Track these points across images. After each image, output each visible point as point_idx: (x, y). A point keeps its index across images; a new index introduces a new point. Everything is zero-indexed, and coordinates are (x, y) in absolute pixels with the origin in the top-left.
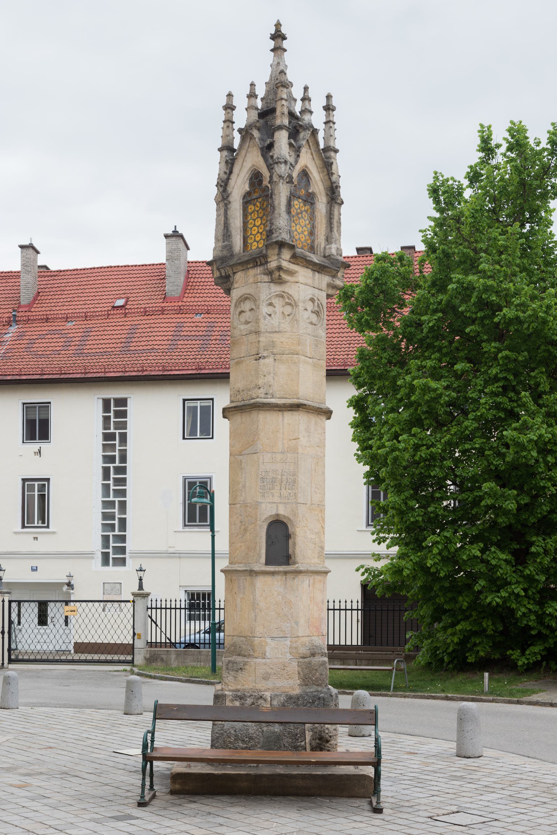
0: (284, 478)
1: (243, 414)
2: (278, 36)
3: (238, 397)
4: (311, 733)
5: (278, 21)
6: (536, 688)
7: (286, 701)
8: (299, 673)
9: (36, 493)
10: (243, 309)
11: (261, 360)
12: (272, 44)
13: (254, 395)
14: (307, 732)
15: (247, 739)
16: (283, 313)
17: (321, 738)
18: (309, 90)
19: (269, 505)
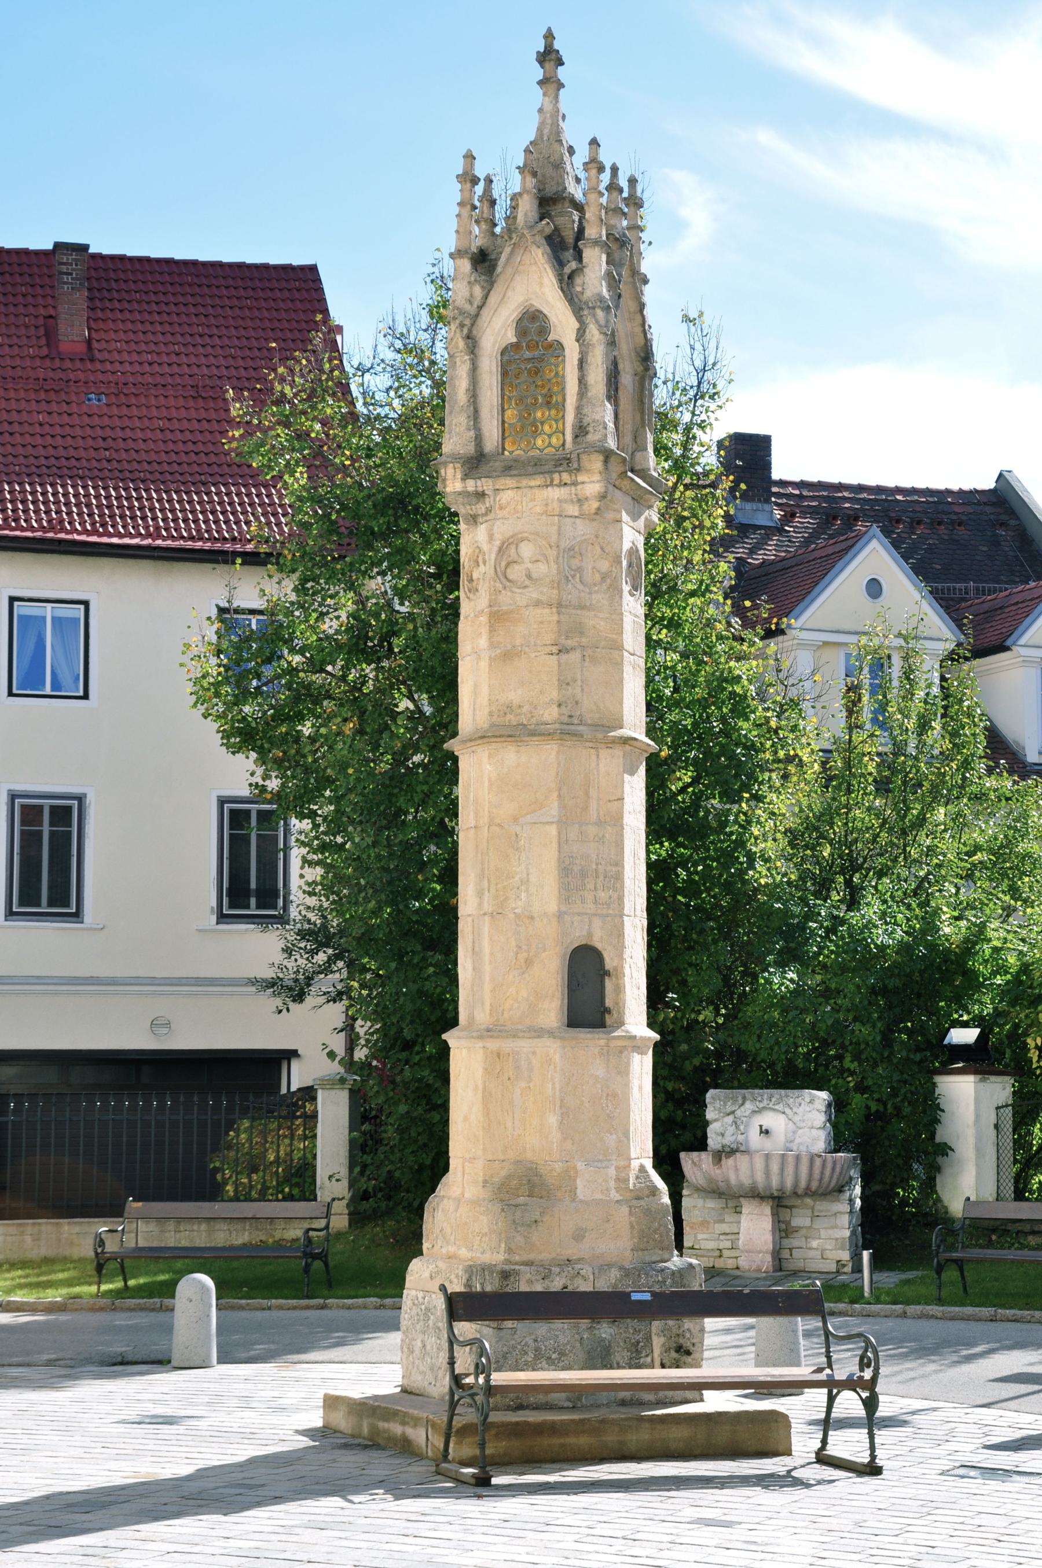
1: (523, 749)
3: (509, 717)
4: (662, 1340)
5: (549, 30)
9: (46, 829)
10: (516, 558)
12: (539, 73)
14: (655, 1338)
17: (679, 1349)
19: (576, 918)
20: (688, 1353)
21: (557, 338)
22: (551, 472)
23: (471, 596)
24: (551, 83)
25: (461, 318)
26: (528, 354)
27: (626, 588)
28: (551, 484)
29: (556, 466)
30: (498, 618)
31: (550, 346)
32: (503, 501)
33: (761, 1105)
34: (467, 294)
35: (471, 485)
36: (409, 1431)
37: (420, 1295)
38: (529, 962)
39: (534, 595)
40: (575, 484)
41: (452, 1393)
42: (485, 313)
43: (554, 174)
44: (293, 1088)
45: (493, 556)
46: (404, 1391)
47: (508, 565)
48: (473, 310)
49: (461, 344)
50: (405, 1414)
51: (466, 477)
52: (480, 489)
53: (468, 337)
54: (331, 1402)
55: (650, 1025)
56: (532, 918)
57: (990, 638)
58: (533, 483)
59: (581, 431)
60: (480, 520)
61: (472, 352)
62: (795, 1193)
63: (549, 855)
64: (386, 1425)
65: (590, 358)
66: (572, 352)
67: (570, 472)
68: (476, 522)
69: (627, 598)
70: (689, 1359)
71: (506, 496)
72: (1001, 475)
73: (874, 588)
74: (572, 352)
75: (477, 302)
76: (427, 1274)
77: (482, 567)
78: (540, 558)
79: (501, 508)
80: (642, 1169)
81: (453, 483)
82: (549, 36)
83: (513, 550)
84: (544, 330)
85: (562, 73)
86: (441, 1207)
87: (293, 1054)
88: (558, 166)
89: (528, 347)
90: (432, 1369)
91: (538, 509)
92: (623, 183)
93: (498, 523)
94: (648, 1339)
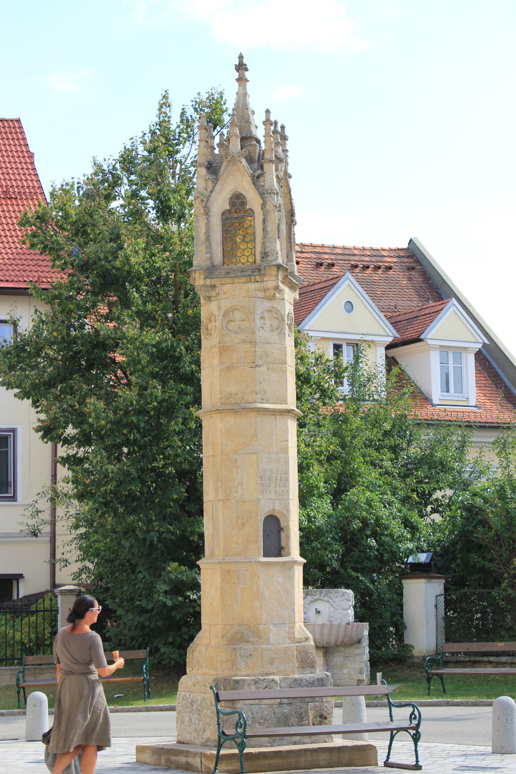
0: (279, 476)
2: (241, 67)
3: (230, 400)
4: (313, 712)
5: (241, 53)
6: (410, 690)
7: (292, 683)
8: (297, 657)
10: (232, 318)
11: (257, 368)
13: (250, 400)
14: (310, 711)
15: (262, 721)
16: (271, 326)
17: (321, 716)
18: (286, 129)
20: (326, 718)
21: (251, 207)
22: (250, 276)
23: (208, 337)
24: (242, 80)
25: (202, 197)
26: (235, 215)
27: (287, 332)
28: (250, 282)
29: (253, 272)
30: (223, 349)
31: (247, 211)
32: (225, 290)
33: (315, 598)
34: (204, 185)
35: (208, 282)
36: (190, 760)
37: (187, 694)
38: (243, 524)
39: (243, 338)
40: (262, 281)
41: (219, 737)
42: (213, 194)
43: (246, 125)
44: (21, 596)
45: (221, 318)
46: (179, 742)
47: (228, 322)
48: (207, 193)
49: (202, 210)
50: (188, 752)
51: (206, 278)
52: (213, 284)
53: (205, 207)
54: (140, 749)
55: (302, 555)
56: (245, 502)
57: (410, 334)
58: (241, 281)
59: (265, 255)
60: (213, 299)
61: (208, 214)
62: (336, 645)
63: (254, 469)
64: (176, 758)
65: (269, 218)
66: (259, 215)
67: (260, 275)
68: (210, 300)
69: (287, 337)
70: (326, 721)
71: (227, 287)
72: (411, 240)
73: (349, 306)
74: (259, 215)
75: (210, 189)
76: (191, 683)
77: (213, 323)
78: (246, 319)
79: (224, 293)
80: (301, 626)
81: (198, 280)
82: (241, 57)
83: (231, 315)
84: (243, 203)
85: (247, 75)
86: (197, 649)
87: (19, 577)
88: (248, 122)
89: (235, 212)
90: (196, 730)
91: (244, 294)
92: (279, 129)
93: (223, 301)
94: (307, 712)
